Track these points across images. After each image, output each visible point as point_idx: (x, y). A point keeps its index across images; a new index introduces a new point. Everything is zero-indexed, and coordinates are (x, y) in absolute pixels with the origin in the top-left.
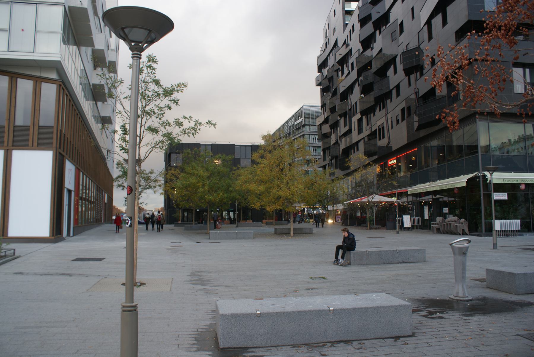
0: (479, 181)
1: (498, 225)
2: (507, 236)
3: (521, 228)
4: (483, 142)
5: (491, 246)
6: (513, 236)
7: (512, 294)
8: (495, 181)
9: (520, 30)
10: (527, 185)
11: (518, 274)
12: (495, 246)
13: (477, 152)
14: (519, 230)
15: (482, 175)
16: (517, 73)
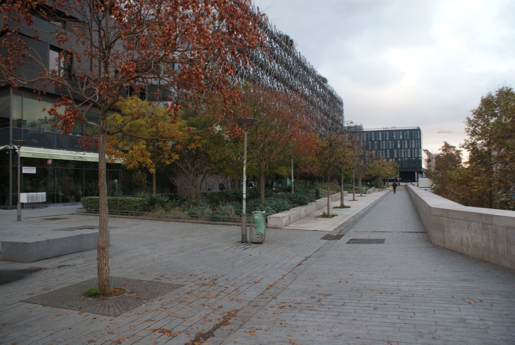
0: (9, 154)
1: (24, 198)
2: (33, 208)
3: (46, 200)
4: (15, 115)
5: (16, 218)
6: (39, 207)
7: (24, 262)
8: (22, 155)
9: (40, 11)
10: (54, 161)
11: (31, 243)
12: (19, 218)
13: (9, 125)
14: (44, 203)
15: (12, 148)
16: (53, 55)
